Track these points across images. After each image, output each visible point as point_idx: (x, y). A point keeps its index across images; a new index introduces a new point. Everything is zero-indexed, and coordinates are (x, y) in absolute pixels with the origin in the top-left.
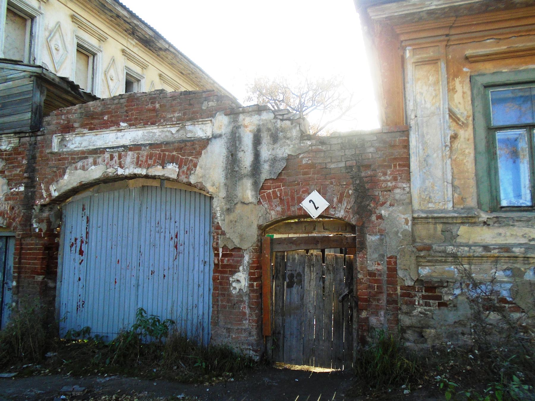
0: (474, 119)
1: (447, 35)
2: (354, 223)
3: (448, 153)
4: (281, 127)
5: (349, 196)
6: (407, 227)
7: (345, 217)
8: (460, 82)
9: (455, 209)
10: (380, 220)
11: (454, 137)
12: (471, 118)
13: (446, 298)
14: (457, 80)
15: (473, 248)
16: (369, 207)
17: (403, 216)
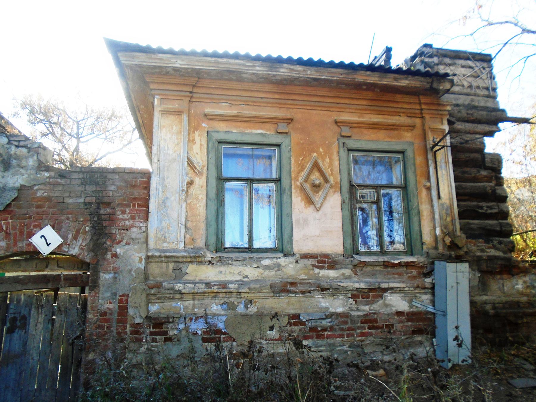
0: (208, 169)
1: (191, 92)
2: (88, 260)
3: (184, 197)
4: (15, 154)
5: (85, 232)
6: (140, 265)
7: (80, 254)
8: (199, 135)
9: (186, 249)
10: (115, 258)
11: (190, 183)
12: (205, 168)
13: (171, 333)
14: (197, 133)
15: (197, 285)
16: (105, 245)
17: (137, 255)
